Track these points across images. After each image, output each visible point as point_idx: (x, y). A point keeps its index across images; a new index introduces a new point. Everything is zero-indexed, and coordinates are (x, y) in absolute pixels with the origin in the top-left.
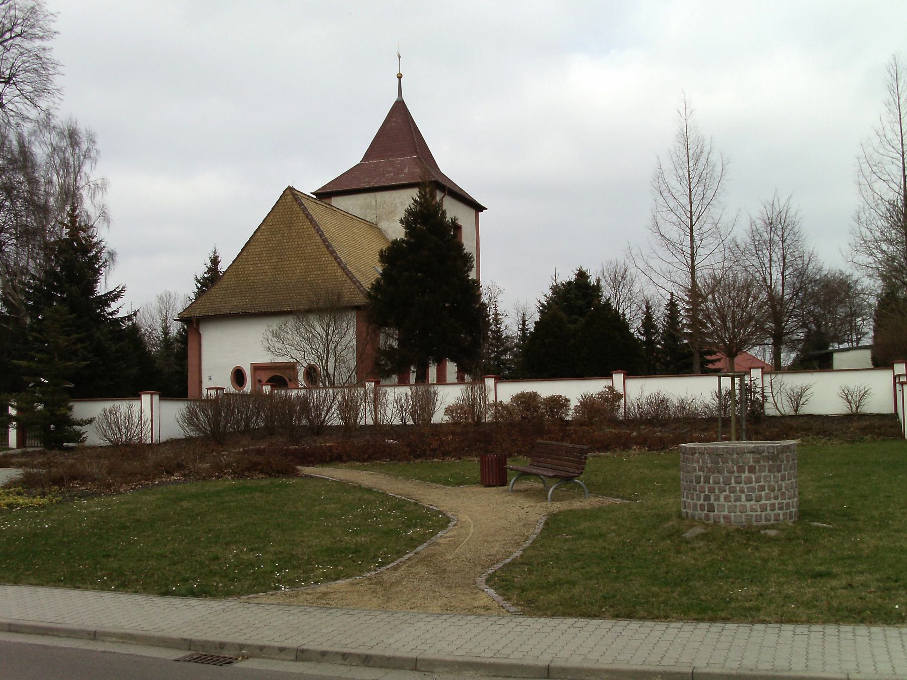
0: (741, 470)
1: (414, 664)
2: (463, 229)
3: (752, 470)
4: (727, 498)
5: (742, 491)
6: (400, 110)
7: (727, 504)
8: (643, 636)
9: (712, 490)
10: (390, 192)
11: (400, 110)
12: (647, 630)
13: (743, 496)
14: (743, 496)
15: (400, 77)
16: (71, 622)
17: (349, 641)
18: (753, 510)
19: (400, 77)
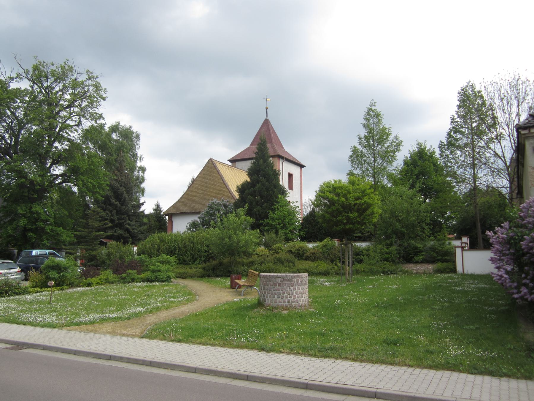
0: (275, 285)
1: (375, 395)
2: (294, 176)
3: (280, 285)
4: (270, 296)
5: (276, 294)
6: (266, 123)
7: (270, 299)
8: (380, 371)
9: (265, 293)
10: (242, 162)
11: (266, 123)
12: (389, 370)
13: (276, 296)
14: (276, 296)
15: (267, 109)
16: (159, 359)
17: (277, 372)
18: (280, 302)
19: (267, 109)
